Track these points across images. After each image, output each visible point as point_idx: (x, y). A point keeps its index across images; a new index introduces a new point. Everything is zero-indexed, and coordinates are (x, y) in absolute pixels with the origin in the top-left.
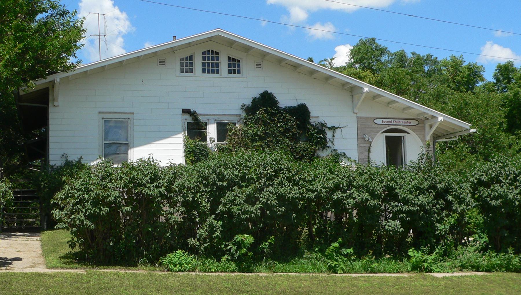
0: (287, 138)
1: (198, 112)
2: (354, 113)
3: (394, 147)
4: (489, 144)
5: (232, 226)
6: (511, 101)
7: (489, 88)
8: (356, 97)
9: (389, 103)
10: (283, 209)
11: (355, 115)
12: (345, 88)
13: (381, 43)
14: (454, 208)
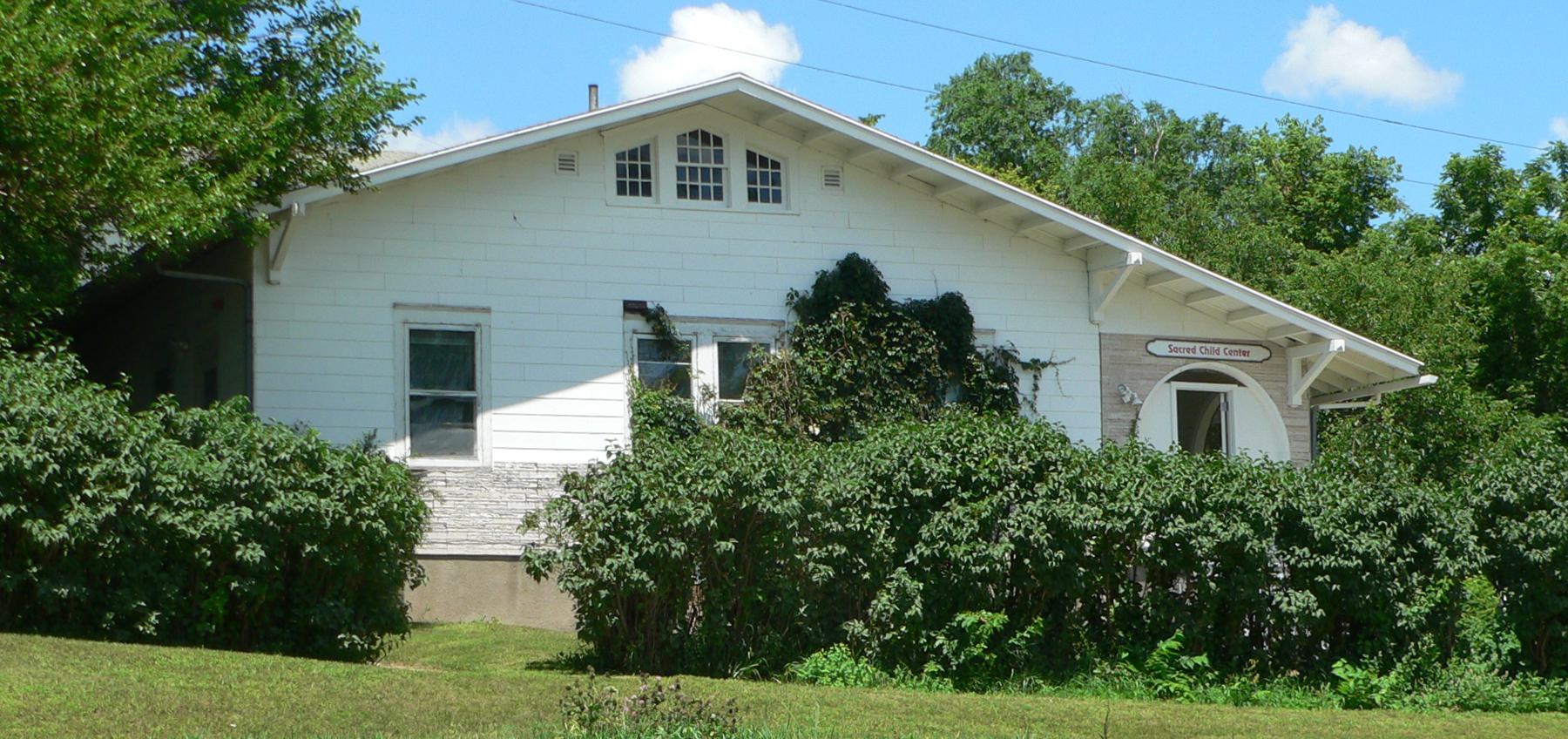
0: (913, 391)
1: (670, 310)
2: (1092, 322)
3: (1201, 419)
4: (1431, 426)
5: (949, 591)
6: (1495, 285)
7: (1415, 237)
8: (1099, 278)
9: (1189, 296)
10: (1060, 554)
11: (1096, 330)
12: (1069, 250)
13: (1051, 69)
14: (1439, 565)
